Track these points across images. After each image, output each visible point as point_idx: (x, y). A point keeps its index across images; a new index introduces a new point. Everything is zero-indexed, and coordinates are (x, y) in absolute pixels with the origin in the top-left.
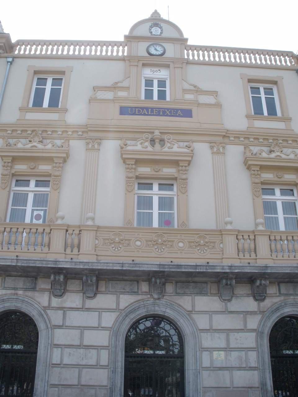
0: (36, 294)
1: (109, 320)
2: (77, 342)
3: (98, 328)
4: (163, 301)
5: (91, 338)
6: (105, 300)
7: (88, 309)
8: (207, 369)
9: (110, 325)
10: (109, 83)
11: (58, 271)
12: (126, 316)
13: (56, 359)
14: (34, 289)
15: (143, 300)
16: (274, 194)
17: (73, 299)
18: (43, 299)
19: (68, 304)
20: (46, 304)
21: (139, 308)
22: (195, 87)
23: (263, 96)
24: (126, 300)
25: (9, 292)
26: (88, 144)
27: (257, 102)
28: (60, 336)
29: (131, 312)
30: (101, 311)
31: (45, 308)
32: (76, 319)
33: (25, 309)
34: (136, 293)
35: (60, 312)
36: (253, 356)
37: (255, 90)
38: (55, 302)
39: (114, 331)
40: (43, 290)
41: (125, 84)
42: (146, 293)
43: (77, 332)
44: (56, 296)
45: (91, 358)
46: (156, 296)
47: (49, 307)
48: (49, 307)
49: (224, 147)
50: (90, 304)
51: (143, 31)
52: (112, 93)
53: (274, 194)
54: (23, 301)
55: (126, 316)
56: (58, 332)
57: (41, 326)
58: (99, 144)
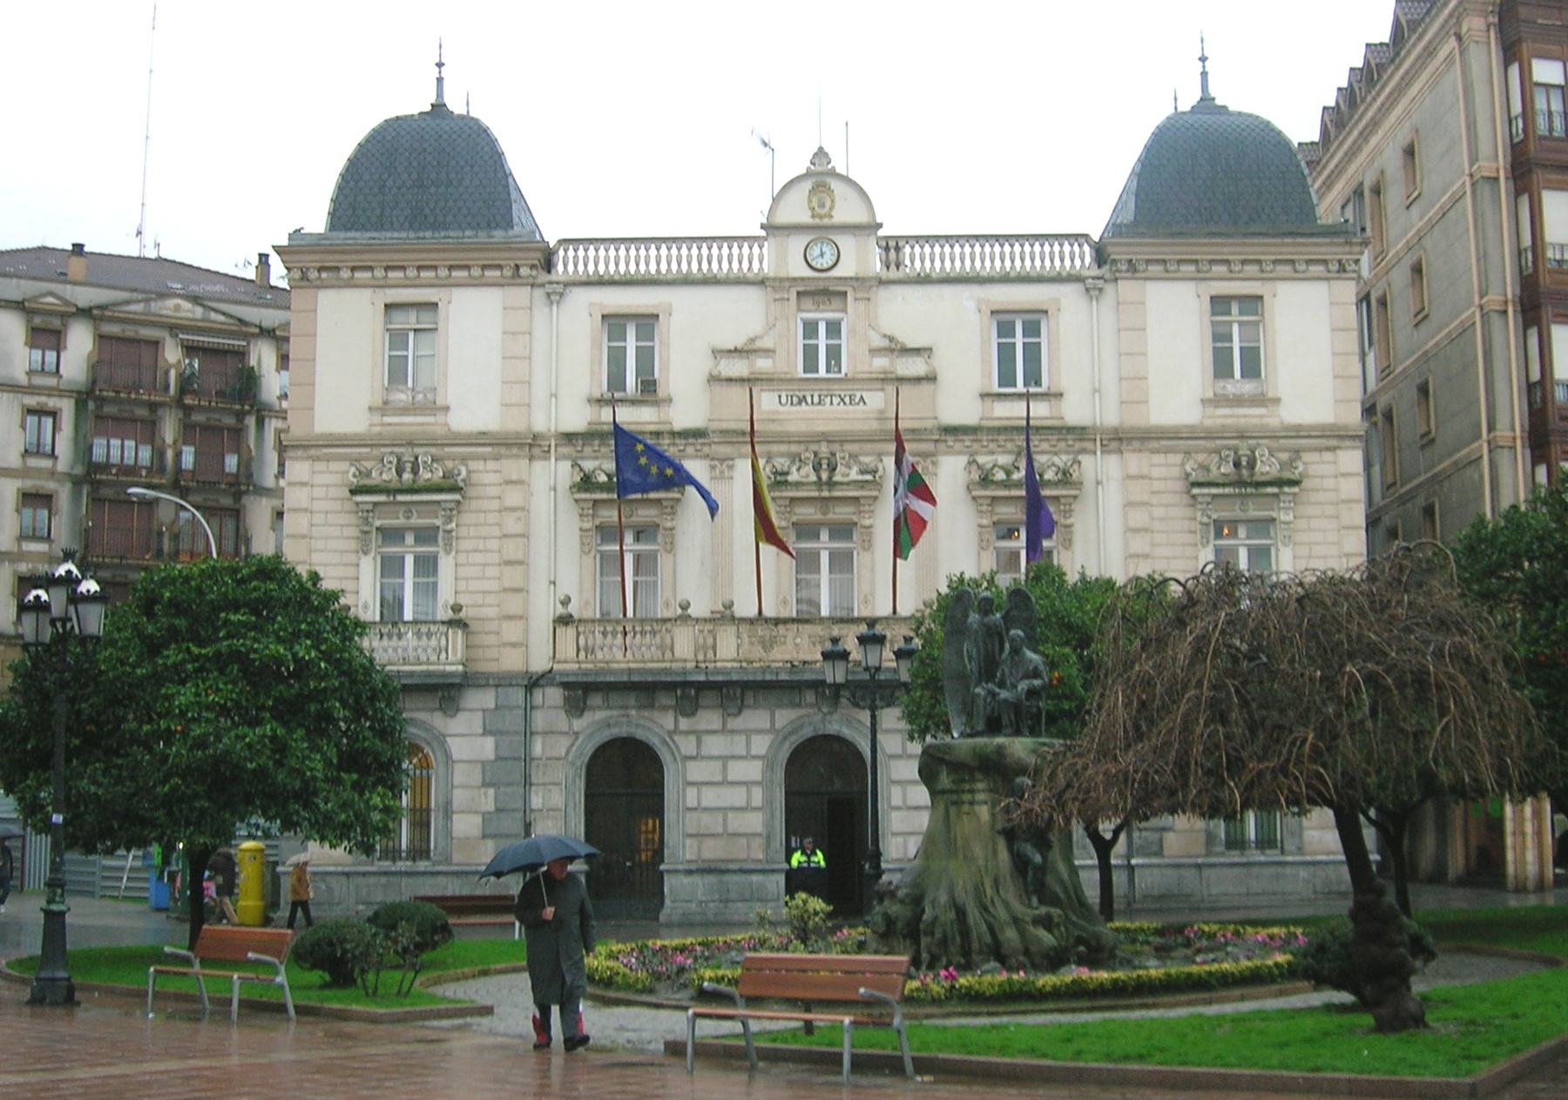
0: (656, 714)
1: (761, 745)
2: (719, 778)
3: (748, 757)
4: (836, 717)
5: (738, 771)
6: (756, 718)
7: (733, 732)
8: (898, 808)
9: (763, 752)
10: (739, 342)
11: (686, 685)
12: (785, 738)
13: (691, 801)
14: (652, 706)
15: (808, 716)
16: (1230, 314)
17: (709, 718)
18: (667, 720)
19: (702, 726)
20: (671, 726)
21: (802, 727)
22: (891, 339)
23: (1019, 340)
24: (784, 717)
25: (615, 713)
26: (713, 468)
27: (1006, 353)
28: (696, 771)
29: (791, 733)
30: (748, 733)
31: (670, 733)
32: (715, 745)
33: (640, 734)
34: (799, 705)
35: (693, 738)
36: (896, 800)
37: (1005, 329)
38: (684, 723)
39: (768, 761)
40: (665, 708)
41: (767, 343)
42: (811, 706)
43: (718, 765)
44: (685, 715)
45: (737, 797)
46: (825, 710)
47: (676, 731)
48: (676, 731)
49: (934, 463)
50: (733, 723)
51: (797, 211)
52: (746, 362)
53: (1230, 314)
54: (638, 726)
55: (785, 738)
56: (691, 765)
57: (666, 757)
58: (731, 467)
